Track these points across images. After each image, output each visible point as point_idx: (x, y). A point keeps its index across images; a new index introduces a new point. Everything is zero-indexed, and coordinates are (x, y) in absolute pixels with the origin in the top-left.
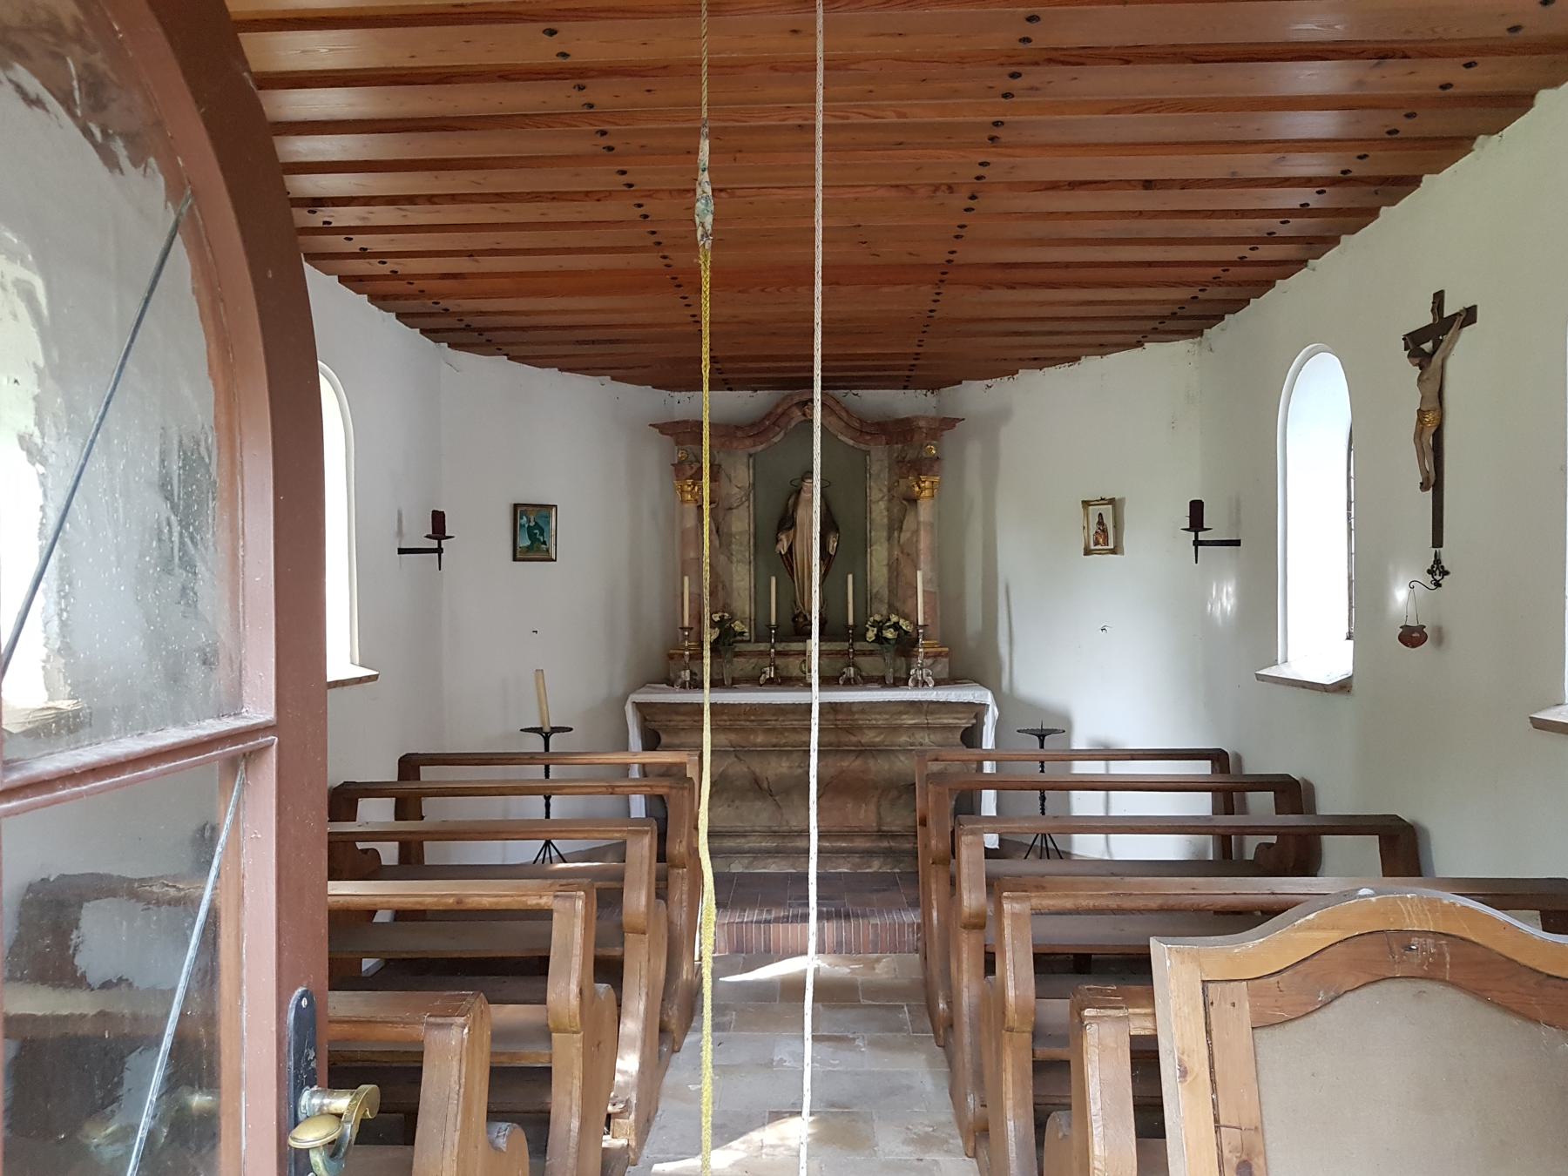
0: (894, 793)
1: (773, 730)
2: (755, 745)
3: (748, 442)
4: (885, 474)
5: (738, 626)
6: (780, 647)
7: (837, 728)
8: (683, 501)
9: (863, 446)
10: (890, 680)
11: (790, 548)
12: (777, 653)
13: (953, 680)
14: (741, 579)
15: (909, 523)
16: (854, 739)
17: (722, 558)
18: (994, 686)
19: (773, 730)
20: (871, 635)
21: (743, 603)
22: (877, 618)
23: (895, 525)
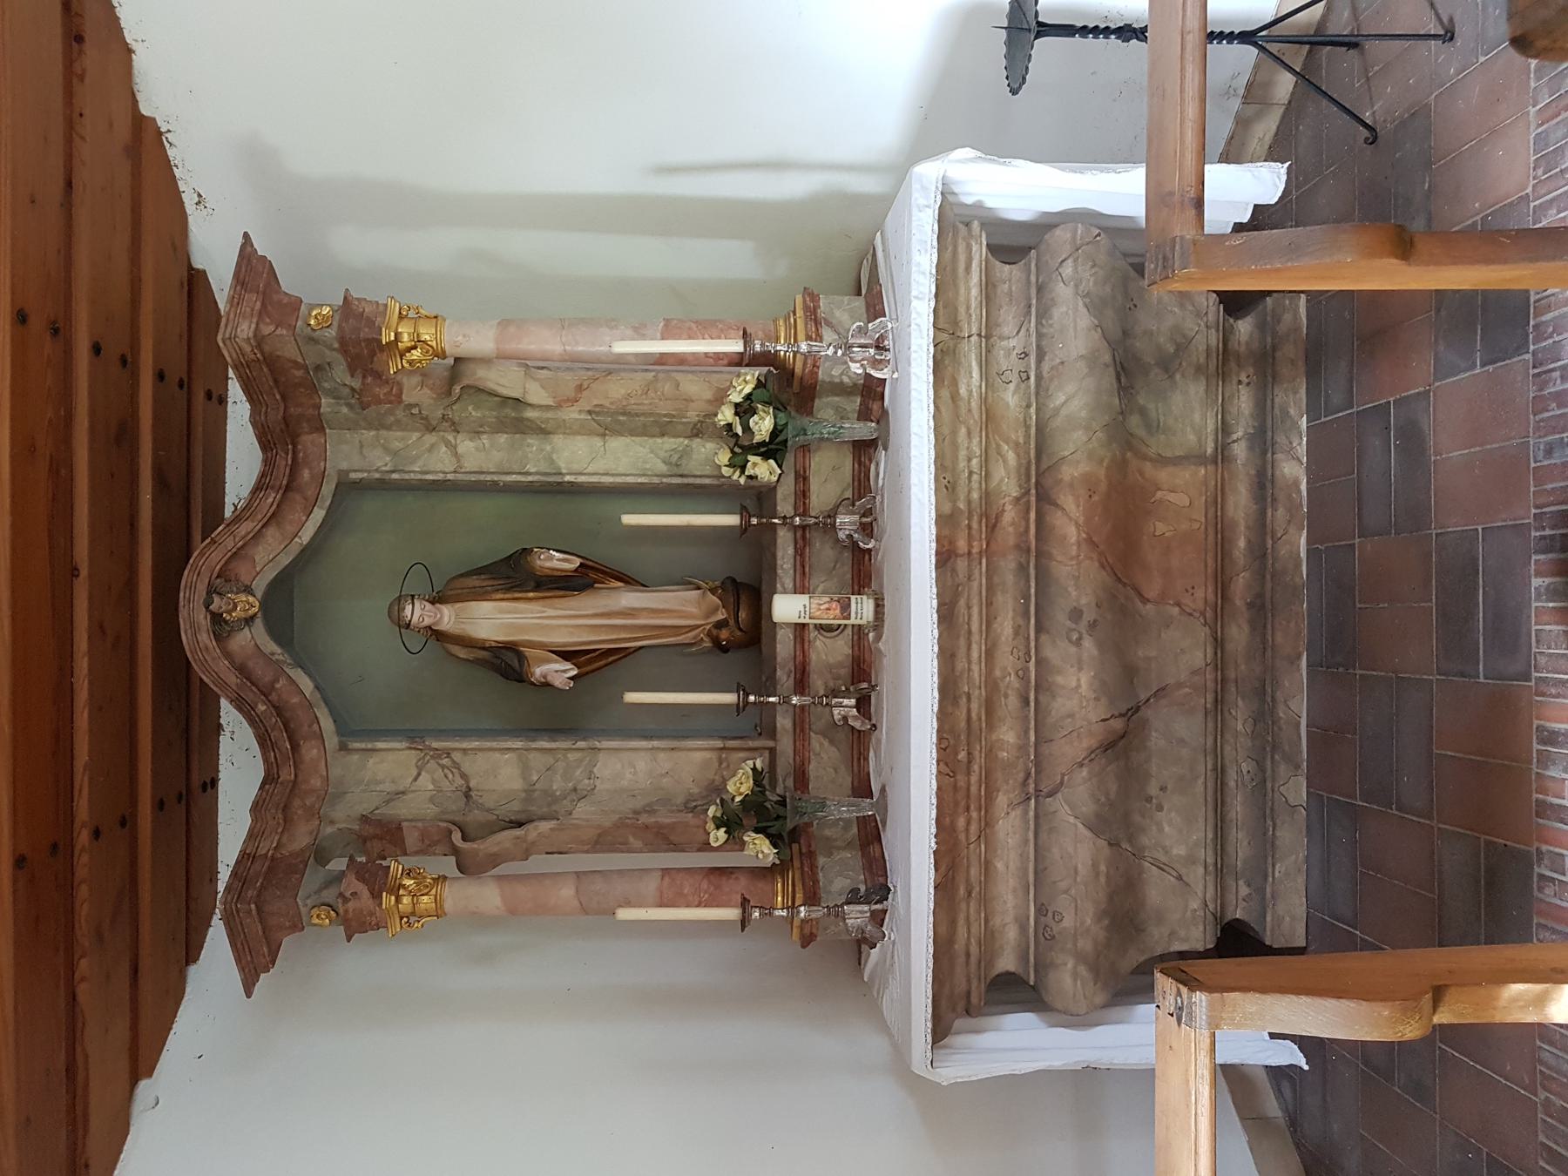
0: (1134, 421)
1: (990, 706)
2: (1022, 748)
3: (310, 752)
4: (396, 438)
5: (740, 786)
6: (784, 678)
7: (988, 552)
8: (439, 913)
9: (328, 489)
10: (865, 430)
11: (566, 655)
12: (801, 686)
13: (870, 292)
14: (627, 770)
15: (506, 380)
16: (1010, 515)
17: (583, 811)
18: (899, 170)
19: (990, 706)
20: (763, 469)
21: (681, 766)
22: (724, 457)
23: (512, 416)
